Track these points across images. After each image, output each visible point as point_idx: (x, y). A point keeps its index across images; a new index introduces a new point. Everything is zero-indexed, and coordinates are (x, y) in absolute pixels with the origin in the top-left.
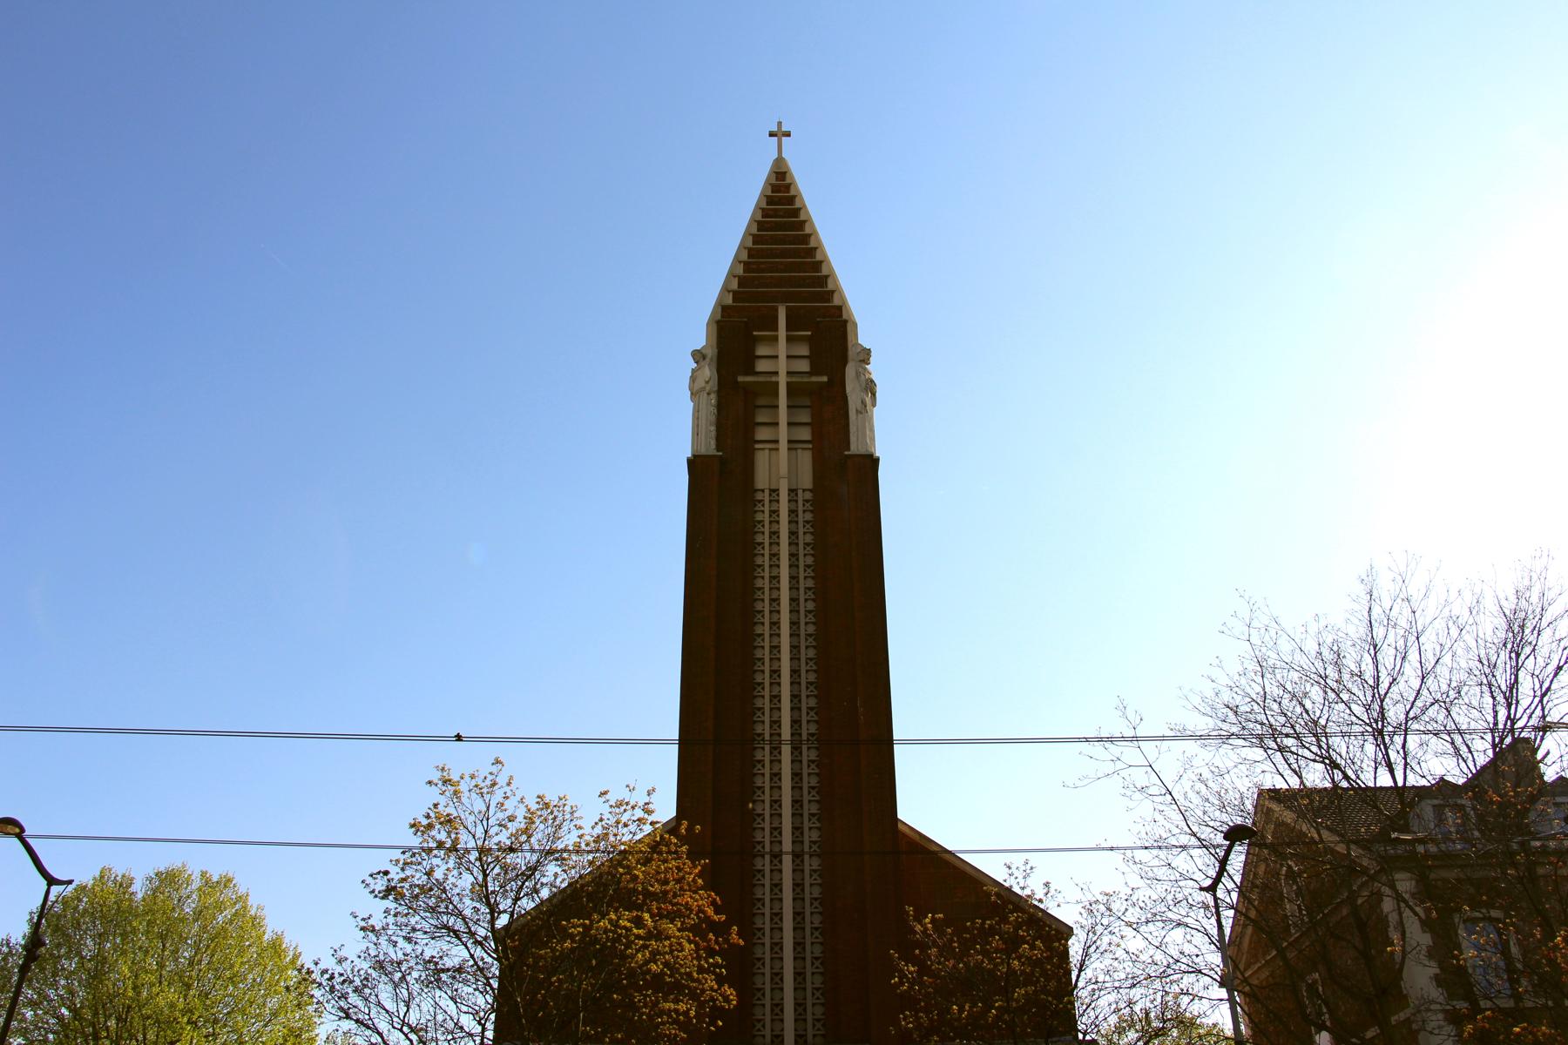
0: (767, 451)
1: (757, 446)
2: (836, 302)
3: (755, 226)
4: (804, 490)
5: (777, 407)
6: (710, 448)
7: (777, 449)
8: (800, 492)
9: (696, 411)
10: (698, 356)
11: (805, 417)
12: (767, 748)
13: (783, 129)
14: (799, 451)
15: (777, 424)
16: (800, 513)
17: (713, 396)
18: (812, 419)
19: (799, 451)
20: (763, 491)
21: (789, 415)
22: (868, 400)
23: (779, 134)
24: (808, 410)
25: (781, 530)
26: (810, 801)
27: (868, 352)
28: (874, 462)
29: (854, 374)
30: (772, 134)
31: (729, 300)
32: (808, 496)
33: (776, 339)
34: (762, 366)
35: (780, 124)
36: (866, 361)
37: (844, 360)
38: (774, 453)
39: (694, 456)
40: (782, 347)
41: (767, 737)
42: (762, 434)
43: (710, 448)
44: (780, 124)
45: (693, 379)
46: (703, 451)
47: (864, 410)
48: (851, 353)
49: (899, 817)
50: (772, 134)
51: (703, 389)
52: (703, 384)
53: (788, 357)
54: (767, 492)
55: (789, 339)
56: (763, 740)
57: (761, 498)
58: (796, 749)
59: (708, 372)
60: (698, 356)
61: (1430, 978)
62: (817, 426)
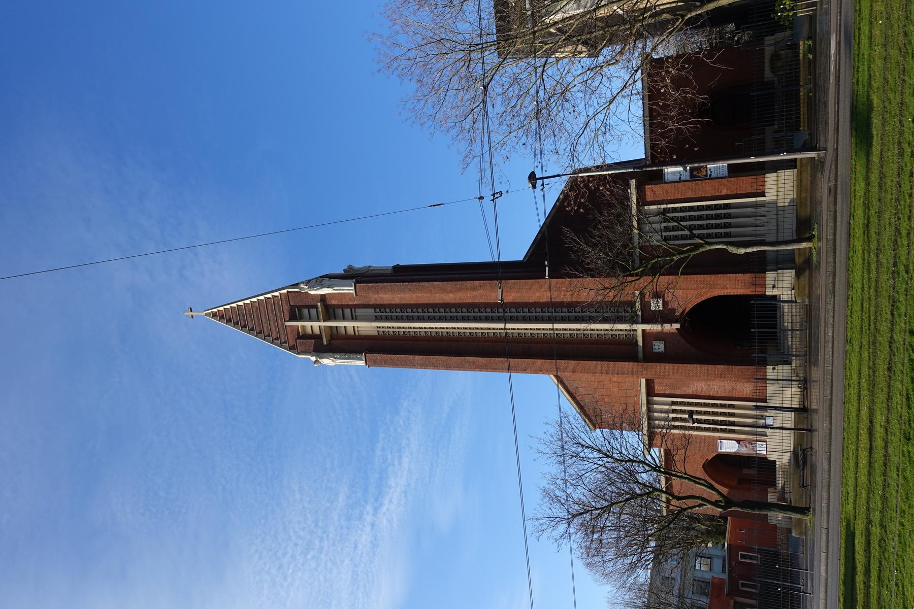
4: (375, 312)
8: (377, 314)
20: (378, 331)
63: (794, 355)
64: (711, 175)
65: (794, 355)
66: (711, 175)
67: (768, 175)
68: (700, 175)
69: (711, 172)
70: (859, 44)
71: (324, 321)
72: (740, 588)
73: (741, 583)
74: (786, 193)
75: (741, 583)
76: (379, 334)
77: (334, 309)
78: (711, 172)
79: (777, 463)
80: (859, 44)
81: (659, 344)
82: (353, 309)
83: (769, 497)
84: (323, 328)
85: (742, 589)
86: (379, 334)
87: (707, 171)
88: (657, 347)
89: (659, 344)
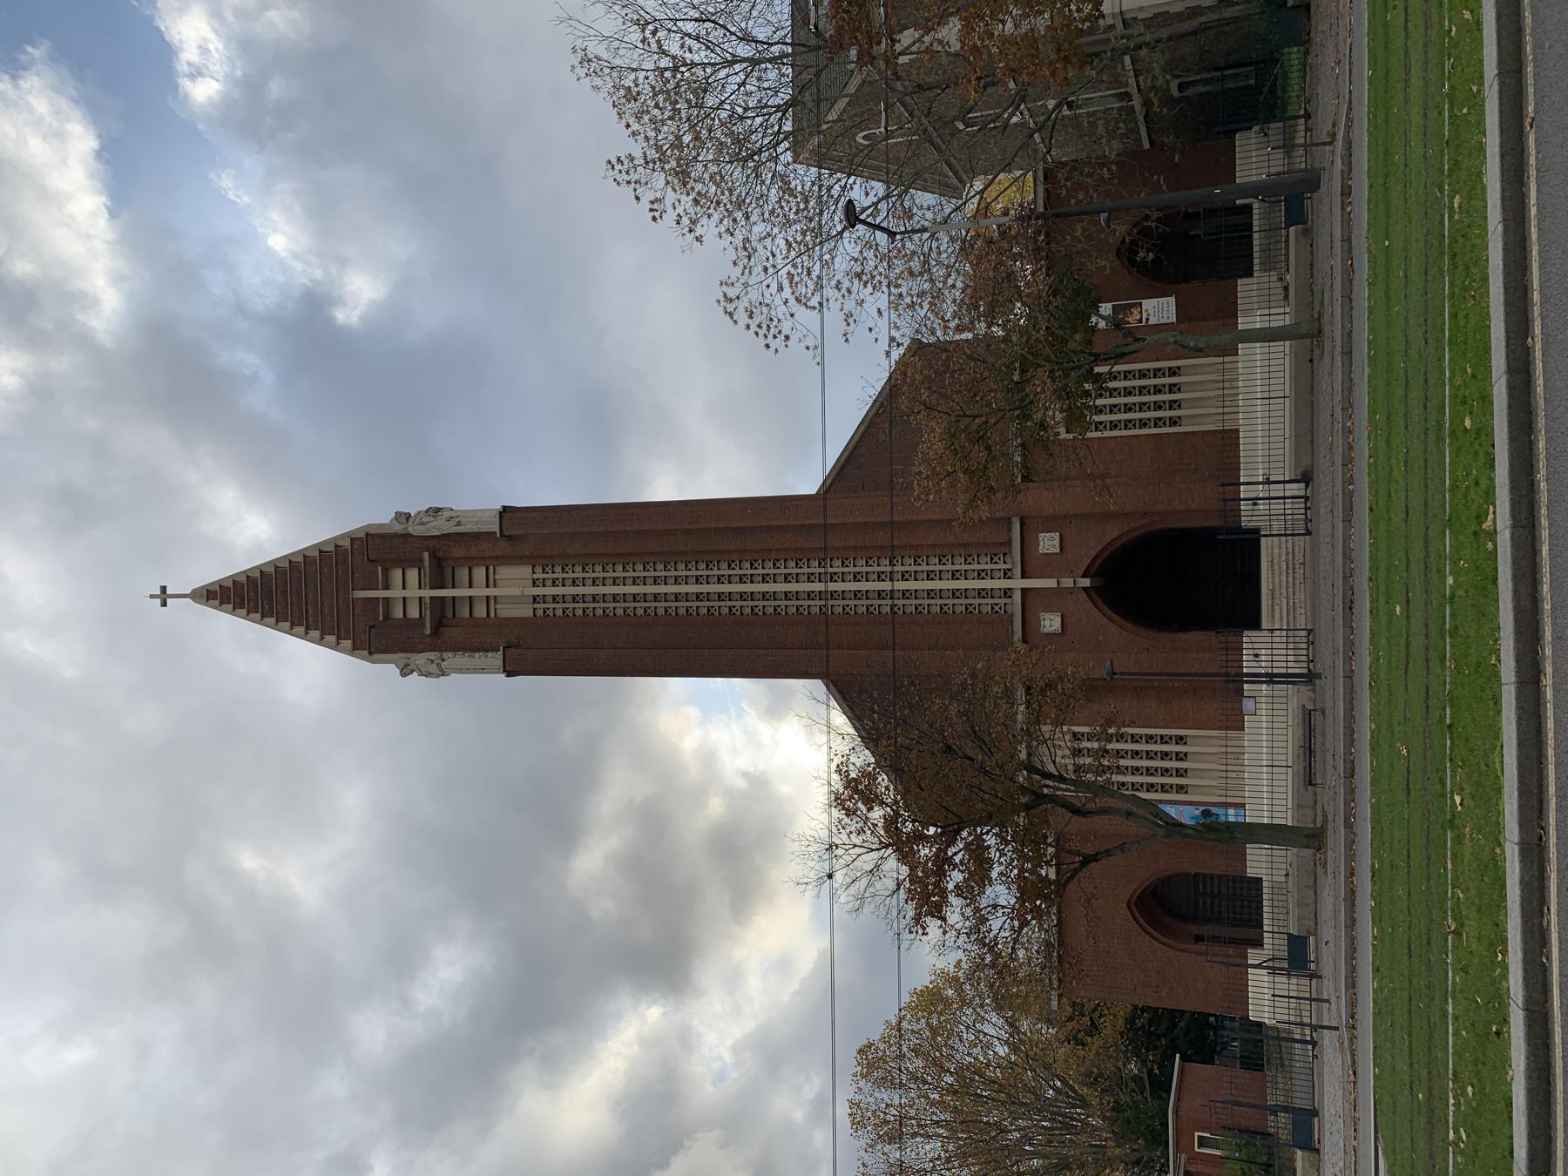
0: (498, 606)
1: (492, 615)
2: (346, 543)
3: (252, 615)
4: (534, 573)
5: (454, 598)
6: (496, 658)
7: (495, 597)
8: (535, 576)
9: (460, 671)
10: (405, 672)
11: (463, 573)
12: (831, 603)
13: (159, 593)
14: (497, 577)
15: (470, 597)
16: (555, 576)
17: (445, 655)
18: (415, 566)
19: (497, 577)
20: (535, 609)
21: (461, 587)
22: (447, 514)
23: (164, 596)
24: (497, 568)
25: (1002, 587)
26: (953, 564)
27: (398, 514)
28: (506, 511)
29: (422, 527)
30: (164, 604)
31: (348, 643)
32: (539, 569)
33: (387, 600)
34: (414, 613)
35: (152, 596)
36: (408, 516)
37: (406, 537)
38: (498, 601)
39: (504, 671)
40: (413, 592)
41: (823, 603)
42: (481, 611)
43: (496, 658)
44: (152, 596)
45: (428, 675)
46: (500, 663)
47: (454, 517)
48: (398, 528)
49: (814, 492)
50: (164, 604)
51: (439, 665)
52: (434, 665)
53: (470, 587)
54: (536, 606)
55: (387, 587)
56: (824, 606)
57: (581, 611)
58: (832, 578)
59: (420, 659)
60: (405, 672)
61: (345, 305)
62: (471, 562)
63: (1297, 1041)
64: (1148, 319)
65: (1297, 1041)
66: (1148, 319)
67: (1246, 633)
68: (1130, 320)
69: (1149, 315)
70: (1386, 76)
71: (431, 588)
72: (1197, 1150)
73: (1199, 1137)
74: (1272, 439)
75: (1199, 1137)
76: (535, 615)
77: (453, 568)
78: (1149, 315)
79: (1265, 884)
80: (1386, 76)
81: (1052, 618)
82: (491, 568)
83: (1248, 851)
84: (428, 601)
85: (1203, 1150)
86: (535, 615)
87: (1141, 313)
88: (1047, 623)
89: (1052, 618)
